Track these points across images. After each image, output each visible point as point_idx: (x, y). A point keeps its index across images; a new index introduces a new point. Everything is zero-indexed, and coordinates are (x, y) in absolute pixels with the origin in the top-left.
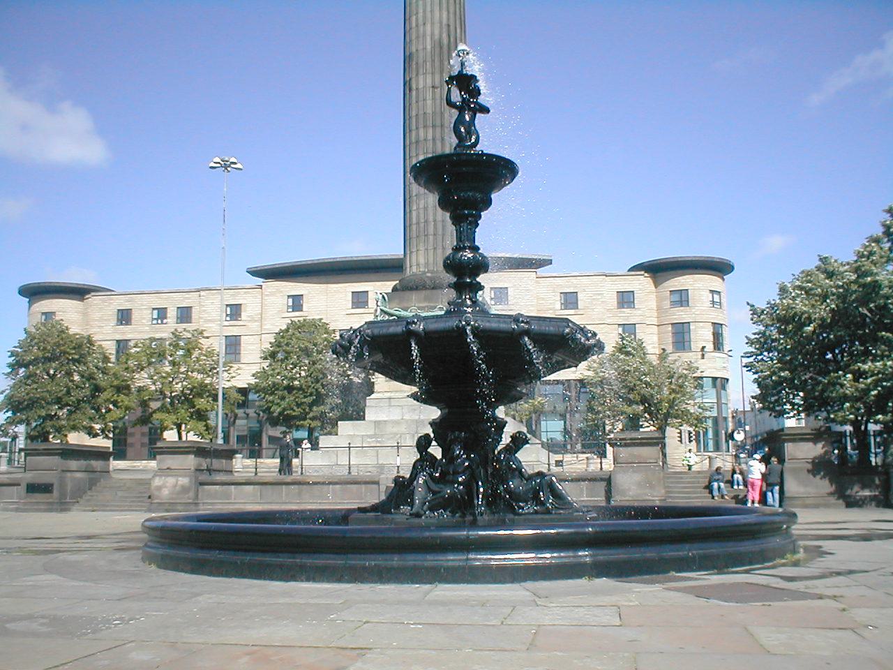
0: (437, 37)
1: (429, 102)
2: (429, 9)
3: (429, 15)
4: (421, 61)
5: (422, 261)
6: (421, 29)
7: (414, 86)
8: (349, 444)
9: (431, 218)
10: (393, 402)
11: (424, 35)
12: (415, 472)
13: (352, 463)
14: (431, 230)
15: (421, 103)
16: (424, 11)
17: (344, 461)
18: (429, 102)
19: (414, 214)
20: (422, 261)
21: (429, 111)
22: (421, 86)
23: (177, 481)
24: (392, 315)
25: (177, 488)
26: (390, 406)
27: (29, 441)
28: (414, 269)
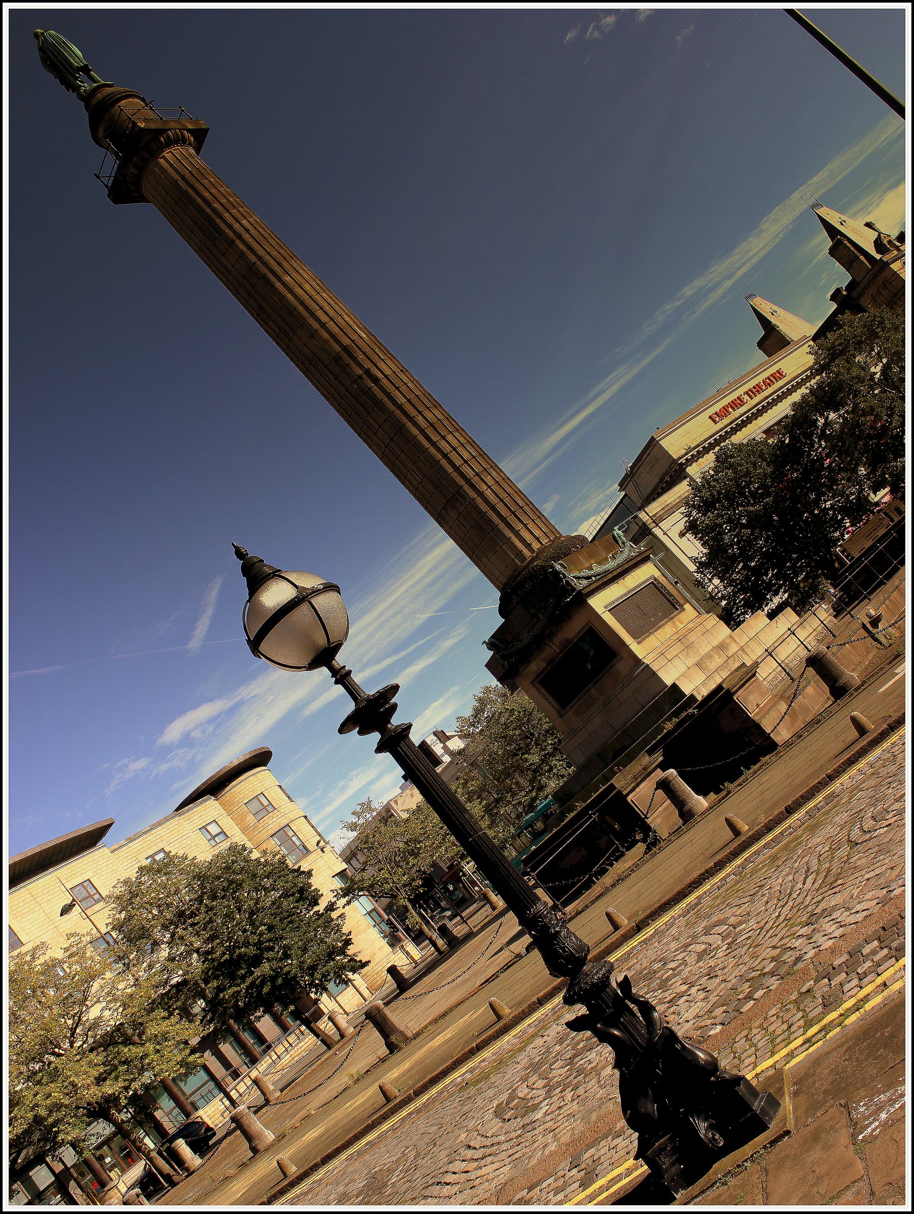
7: (380, 375)
19: (488, 493)
22: (388, 372)
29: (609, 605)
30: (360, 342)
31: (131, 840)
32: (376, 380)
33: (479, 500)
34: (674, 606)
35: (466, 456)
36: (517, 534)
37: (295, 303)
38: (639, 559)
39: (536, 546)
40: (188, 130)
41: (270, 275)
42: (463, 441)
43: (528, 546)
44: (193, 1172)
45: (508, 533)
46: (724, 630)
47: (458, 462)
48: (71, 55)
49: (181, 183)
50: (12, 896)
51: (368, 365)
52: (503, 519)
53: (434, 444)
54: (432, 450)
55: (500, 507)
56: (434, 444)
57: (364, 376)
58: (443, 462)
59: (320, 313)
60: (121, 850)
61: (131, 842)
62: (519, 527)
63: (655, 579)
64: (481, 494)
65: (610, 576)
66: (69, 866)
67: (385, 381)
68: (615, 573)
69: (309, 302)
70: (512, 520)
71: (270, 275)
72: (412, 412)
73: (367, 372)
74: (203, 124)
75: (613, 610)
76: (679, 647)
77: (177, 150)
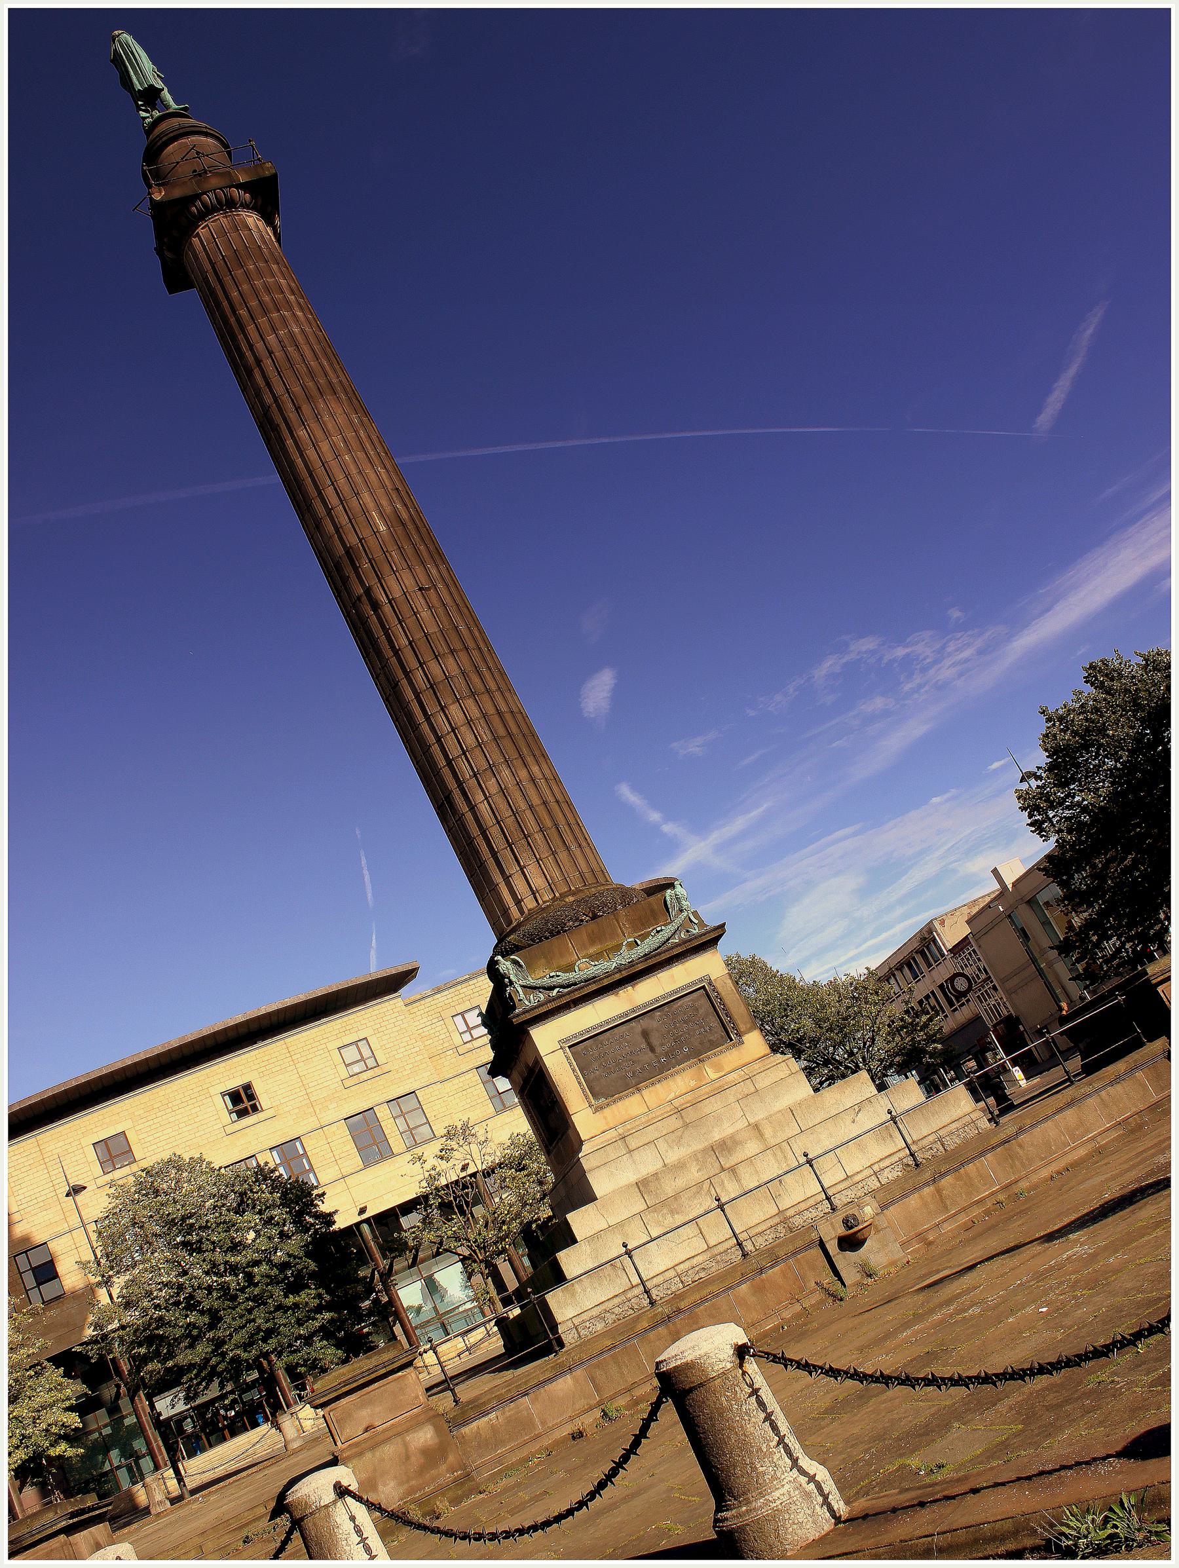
0: (388, 509)
1: (425, 614)
2: (354, 471)
3: (358, 479)
4: (378, 554)
5: (538, 882)
6: (354, 503)
7: (383, 599)
8: (625, 1245)
9: (523, 805)
10: (633, 1143)
11: (365, 512)
12: (471, 1414)
13: (826, 1186)
14: (531, 824)
15: (411, 622)
16: (347, 476)
17: (718, 1233)
18: (425, 614)
19: (484, 808)
20: (538, 882)
21: (432, 629)
22: (397, 593)
23: (406, 1445)
24: (552, 988)
25: (413, 1459)
26: (630, 1151)
27: (30, 1493)
28: (529, 903)
29: (568, 1040)
30: (372, 542)
31: (439, 991)
32: (376, 606)
33: (469, 816)
34: (729, 1033)
35: (469, 740)
36: (507, 879)
37: (304, 473)
38: (618, 977)
39: (529, 903)
40: (239, 186)
41: (283, 426)
42: (503, 708)
43: (518, 902)
44: (1012, 1107)
45: (498, 878)
46: (802, 1088)
47: (454, 751)
48: (136, 73)
49: (211, 278)
50: (30, 1142)
51: (372, 581)
52: (494, 854)
53: (428, 718)
54: (425, 728)
55: (494, 832)
56: (428, 718)
57: (364, 598)
58: (436, 749)
59: (329, 492)
60: (423, 1002)
61: (439, 992)
62: (513, 869)
63: (710, 984)
64: (473, 808)
65: (594, 987)
66: (345, 1019)
67: (387, 609)
68: (606, 982)
69: (320, 471)
70: (506, 856)
71: (283, 426)
72: (412, 663)
73: (368, 591)
74: (268, 169)
75: (577, 1047)
76: (674, 1122)
77: (220, 220)
